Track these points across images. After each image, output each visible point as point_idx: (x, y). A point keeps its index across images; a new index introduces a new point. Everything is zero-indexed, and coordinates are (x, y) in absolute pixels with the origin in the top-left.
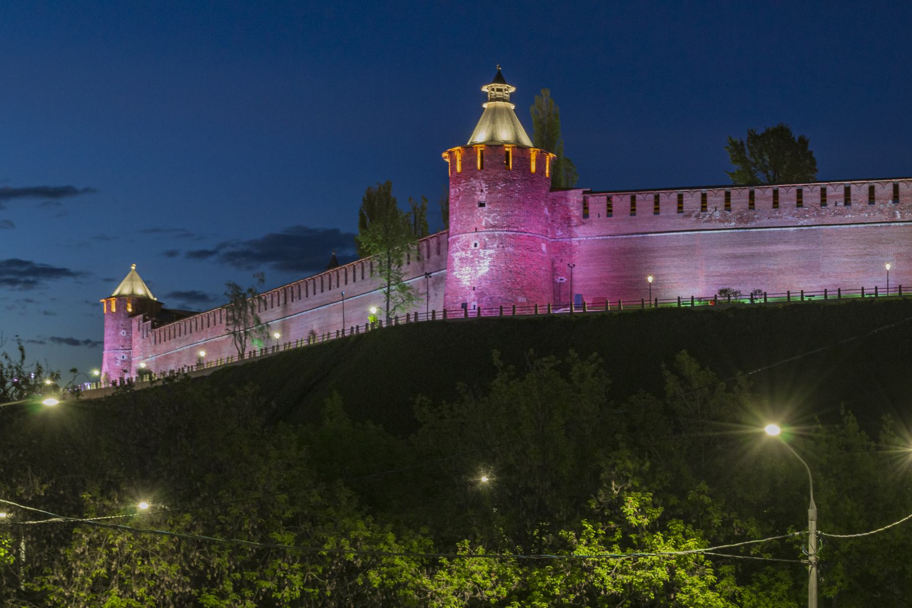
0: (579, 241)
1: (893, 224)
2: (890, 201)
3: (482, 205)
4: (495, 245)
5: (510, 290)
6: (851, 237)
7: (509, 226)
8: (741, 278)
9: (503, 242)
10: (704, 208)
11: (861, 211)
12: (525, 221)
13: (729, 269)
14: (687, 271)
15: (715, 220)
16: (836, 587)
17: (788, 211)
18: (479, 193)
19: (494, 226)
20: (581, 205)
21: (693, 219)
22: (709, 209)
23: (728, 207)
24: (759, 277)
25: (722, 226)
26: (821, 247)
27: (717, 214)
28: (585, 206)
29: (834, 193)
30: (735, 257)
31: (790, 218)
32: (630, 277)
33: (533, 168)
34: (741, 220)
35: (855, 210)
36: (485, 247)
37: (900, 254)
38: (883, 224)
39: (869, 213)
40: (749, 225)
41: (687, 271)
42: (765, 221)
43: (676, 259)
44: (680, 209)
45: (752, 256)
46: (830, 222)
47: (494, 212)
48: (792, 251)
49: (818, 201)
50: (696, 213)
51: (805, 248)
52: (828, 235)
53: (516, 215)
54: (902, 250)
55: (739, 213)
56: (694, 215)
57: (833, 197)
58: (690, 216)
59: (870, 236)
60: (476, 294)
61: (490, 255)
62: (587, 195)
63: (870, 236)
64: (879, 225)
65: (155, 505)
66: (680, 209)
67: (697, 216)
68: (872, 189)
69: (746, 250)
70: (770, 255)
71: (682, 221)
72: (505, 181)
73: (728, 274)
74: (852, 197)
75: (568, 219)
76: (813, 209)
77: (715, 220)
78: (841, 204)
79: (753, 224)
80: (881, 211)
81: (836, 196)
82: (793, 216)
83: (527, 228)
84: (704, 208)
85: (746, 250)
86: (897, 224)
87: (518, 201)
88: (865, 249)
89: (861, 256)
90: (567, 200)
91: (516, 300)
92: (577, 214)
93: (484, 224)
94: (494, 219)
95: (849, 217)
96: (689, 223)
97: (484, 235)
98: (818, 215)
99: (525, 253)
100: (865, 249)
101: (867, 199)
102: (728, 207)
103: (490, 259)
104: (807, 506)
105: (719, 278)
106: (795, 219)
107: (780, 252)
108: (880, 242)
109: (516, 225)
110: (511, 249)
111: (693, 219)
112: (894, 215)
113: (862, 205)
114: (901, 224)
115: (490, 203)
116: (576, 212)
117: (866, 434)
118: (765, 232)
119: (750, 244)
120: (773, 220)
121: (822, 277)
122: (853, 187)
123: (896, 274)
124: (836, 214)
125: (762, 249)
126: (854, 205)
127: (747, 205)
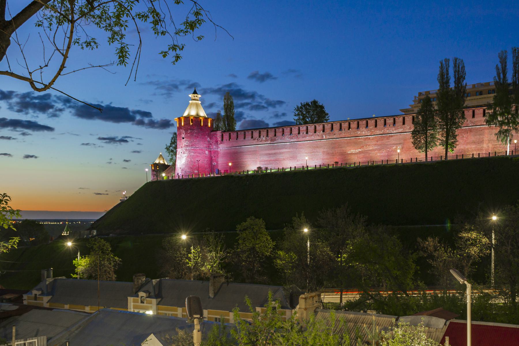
0: (220, 150)
1: (322, 140)
2: (322, 132)
3: (183, 138)
4: (187, 153)
5: (192, 168)
6: (308, 146)
7: (192, 146)
8: (271, 162)
9: (190, 152)
10: (260, 137)
11: (312, 136)
12: (198, 143)
13: (267, 159)
14: (253, 160)
15: (263, 141)
16: (409, 279)
17: (287, 136)
18: (182, 134)
19: (187, 146)
20: (221, 136)
21: (256, 140)
22: (261, 136)
23: (267, 136)
24: (277, 161)
25: (265, 143)
26: (297, 150)
27: (264, 139)
28: (222, 136)
29: (302, 129)
30: (270, 154)
31: (288, 139)
32: (235, 162)
33: (209, 125)
34: (272, 140)
35: (310, 135)
36: (184, 153)
37: (324, 152)
38: (319, 140)
39: (314, 136)
40: (274, 142)
41: (253, 160)
42: (280, 141)
43: (250, 155)
44: (252, 137)
45: (275, 154)
46: (301, 140)
47: (187, 141)
48: (288, 152)
49: (297, 132)
50: (257, 138)
51: (292, 150)
52: (300, 145)
53: (195, 142)
54: (325, 150)
55: (271, 138)
56: (256, 139)
57: (302, 131)
58: (255, 139)
59: (314, 145)
60: (181, 170)
61: (185, 156)
62: (223, 133)
63: (314, 145)
64: (317, 141)
65: (451, 225)
66: (252, 137)
67: (258, 139)
68: (315, 127)
69: (273, 152)
70: (281, 153)
71: (253, 141)
72: (191, 129)
73: (267, 161)
74: (308, 131)
75: (217, 142)
76: (295, 135)
77: (263, 141)
78: (305, 133)
79: (276, 142)
80: (318, 135)
81: (303, 130)
82: (289, 138)
83: (199, 146)
84: (260, 137)
85: (273, 152)
86: (324, 140)
87: (196, 137)
88: (312, 150)
89: (311, 153)
90: (217, 135)
91: (194, 172)
92: (220, 140)
93: (184, 145)
94: (187, 143)
95: (307, 138)
96: (255, 142)
97: (184, 149)
98: (297, 138)
99: (198, 155)
100: (312, 150)
101: (314, 131)
102: (267, 136)
103: (185, 158)
104: (78, 252)
105: (264, 162)
106: (289, 139)
107: (284, 152)
108: (317, 147)
109: (195, 145)
110: (192, 154)
111: (256, 140)
112: (323, 137)
113: (312, 133)
114: (325, 140)
115: (186, 138)
116: (219, 139)
117: (240, 224)
118: (279, 145)
119: (274, 149)
120: (282, 140)
121: (297, 161)
122: (309, 126)
123: (322, 159)
124: (303, 137)
125: (278, 151)
126: (309, 133)
127: (273, 135)
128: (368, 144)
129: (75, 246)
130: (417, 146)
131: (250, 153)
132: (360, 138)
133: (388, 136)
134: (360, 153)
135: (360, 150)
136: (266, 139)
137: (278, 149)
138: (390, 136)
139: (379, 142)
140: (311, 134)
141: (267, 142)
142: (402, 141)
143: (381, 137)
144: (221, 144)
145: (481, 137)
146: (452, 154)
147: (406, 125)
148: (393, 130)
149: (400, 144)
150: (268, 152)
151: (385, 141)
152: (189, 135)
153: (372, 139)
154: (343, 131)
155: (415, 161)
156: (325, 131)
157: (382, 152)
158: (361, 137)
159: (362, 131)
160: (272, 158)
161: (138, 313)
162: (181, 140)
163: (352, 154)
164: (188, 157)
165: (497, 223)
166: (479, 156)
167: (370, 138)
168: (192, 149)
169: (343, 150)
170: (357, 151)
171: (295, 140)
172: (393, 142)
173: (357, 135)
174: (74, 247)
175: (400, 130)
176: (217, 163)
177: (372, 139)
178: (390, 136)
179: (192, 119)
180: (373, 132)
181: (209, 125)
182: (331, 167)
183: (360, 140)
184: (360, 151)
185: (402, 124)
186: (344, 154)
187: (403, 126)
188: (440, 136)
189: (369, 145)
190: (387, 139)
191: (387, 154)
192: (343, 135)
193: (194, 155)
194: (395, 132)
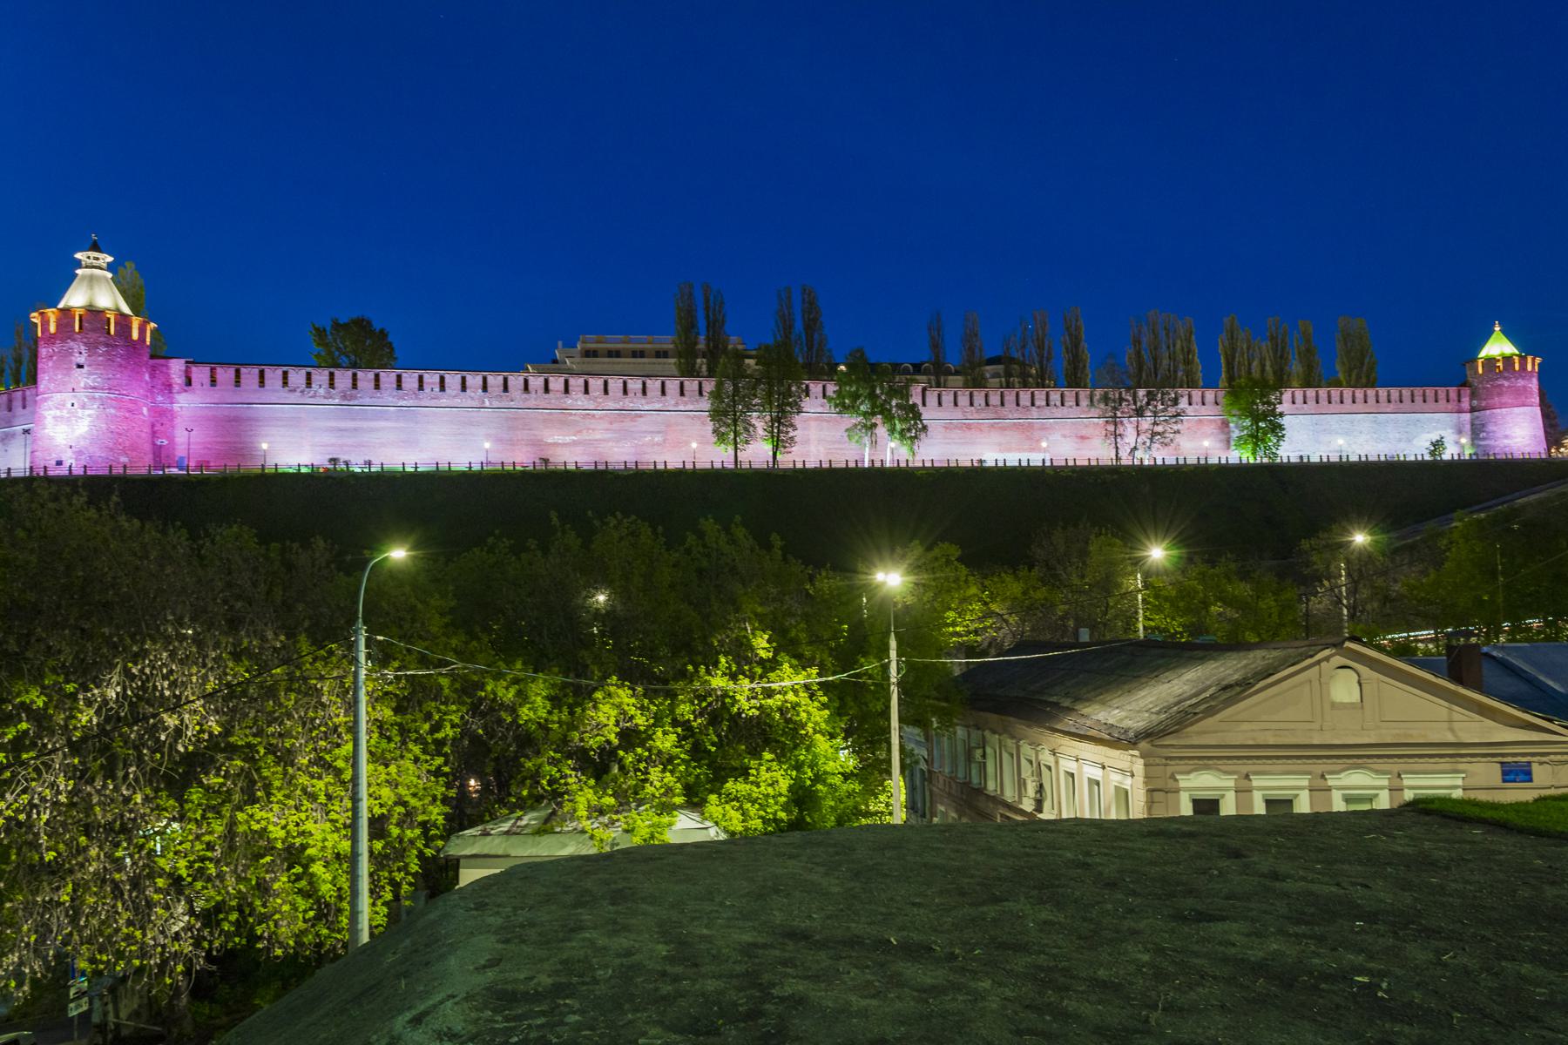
0: (181, 407)
2: (480, 391)
3: (80, 366)
4: (95, 406)
5: (111, 449)
7: (110, 389)
9: (103, 403)
11: (455, 397)
13: (333, 441)
19: (94, 388)
22: (313, 386)
23: (332, 385)
25: (326, 402)
27: (322, 391)
30: (340, 430)
31: (390, 399)
32: (235, 443)
34: (344, 397)
36: (83, 407)
40: (351, 403)
42: (367, 401)
45: (355, 430)
49: (416, 385)
56: (299, 390)
58: (295, 391)
60: (74, 453)
67: (302, 392)
70: (372, 430)
71: (287, 395)
72: (107, 345)
73: (332, 445)
80: (472, 398)
81: (433, 383)
87: (121, 366)
93: (82, 385)
94: (94, 381)
95: (444, 402)
96: (293, 397)
98: (416, 398)
101: (459, 387)
110: (113, 411)
111: (298, 394)
112: (483, 402)
115: (89, 365)
119: (353, 419)
121: (421, 451)
125: (365, 424)
128: (592, 427)
129: (1178, 539)
130: (721, 437)
131: (280, 423)
132: (571, 414)
133: (635, 413)
134: (575, 443)
135: (574, 438)
136: (329, 393)
137: (366, 419)
138: (637, 416)
139: (616, 426)
140: (454, 393)
141: (331, 402)
142: (663, 428)
143: (619, 415)
144: (184, 394)
145: (806, 433)
146: (786, 460)
147: (668, 398)
148: (641, 403)
149: (659, 432)
150: (333, 424)
151: (628, 424)
152: (101, 358)
153: (600, 418)
154: (533, 395)
155: (692, 467)
156: (489, 389)
157: (623, 447)
158: (574, 412)
159: (576, 400)
160: (350, 441)
161: (899, 684)
162: (70, 369)
163: (556, 444)
164: (98, 417)
165: (1365, 528)
166: (111, 471)
167: (594, 416)
168: (112, 399)
169: (535, 435)
170: (568, 439)
171: (411, 403)
172: (644, 428)
173: (564, 406)
174: (870, 569)
175: (657, 406)
176: (171, 439)
177: (600, 418)
178: (637, 416)
179: (81, 316)
180: (600, 403)
181: (135, 335)
182: (304, 470)
183: (572, 418)
184: (574, 441)
185: (621, 394)
186: (537, 443)
187: (663, 398)
188: (759, 422)
189: (593, 430)
190: (632, 421)
191: (633, 450)
192: (532, 403)
193: (118, 414)
194: (647, 408)
